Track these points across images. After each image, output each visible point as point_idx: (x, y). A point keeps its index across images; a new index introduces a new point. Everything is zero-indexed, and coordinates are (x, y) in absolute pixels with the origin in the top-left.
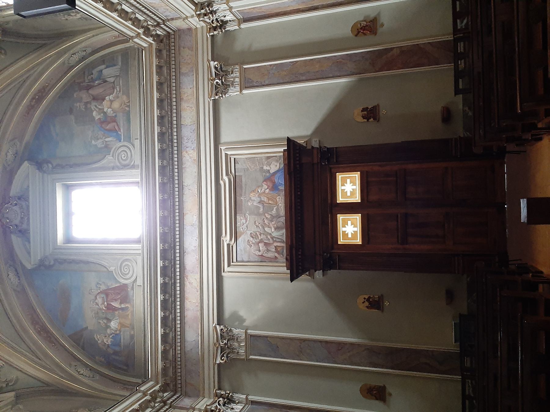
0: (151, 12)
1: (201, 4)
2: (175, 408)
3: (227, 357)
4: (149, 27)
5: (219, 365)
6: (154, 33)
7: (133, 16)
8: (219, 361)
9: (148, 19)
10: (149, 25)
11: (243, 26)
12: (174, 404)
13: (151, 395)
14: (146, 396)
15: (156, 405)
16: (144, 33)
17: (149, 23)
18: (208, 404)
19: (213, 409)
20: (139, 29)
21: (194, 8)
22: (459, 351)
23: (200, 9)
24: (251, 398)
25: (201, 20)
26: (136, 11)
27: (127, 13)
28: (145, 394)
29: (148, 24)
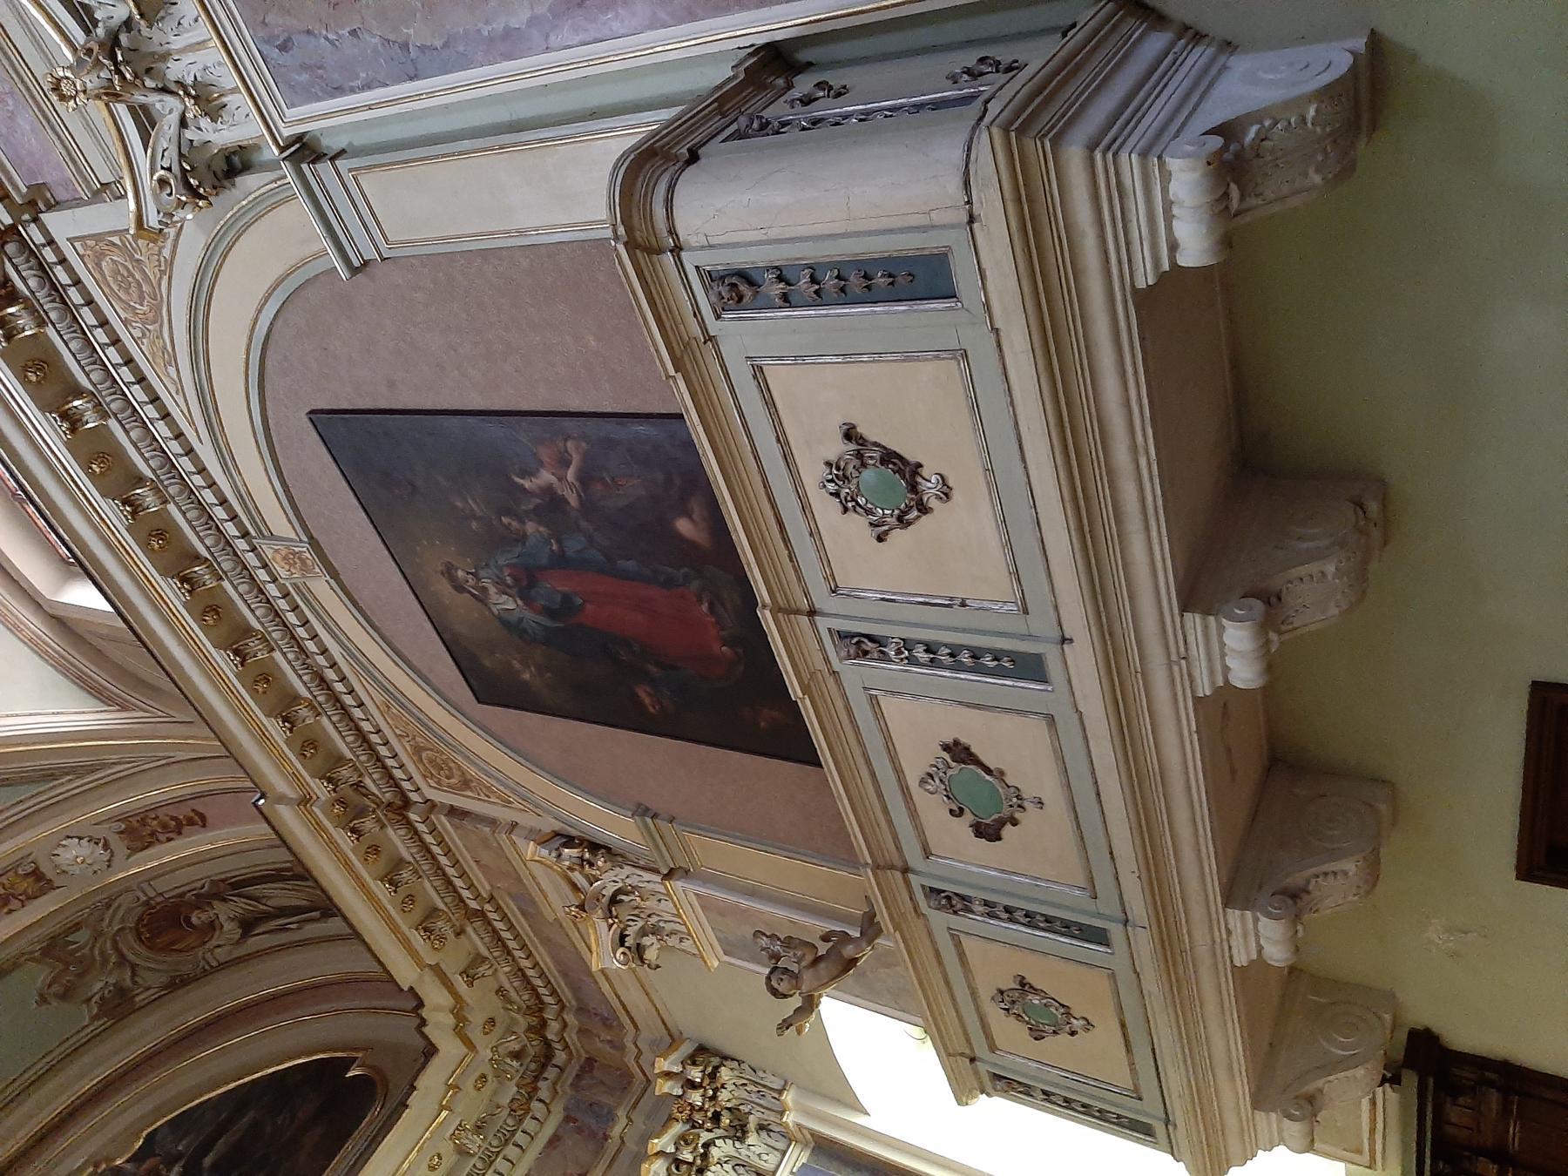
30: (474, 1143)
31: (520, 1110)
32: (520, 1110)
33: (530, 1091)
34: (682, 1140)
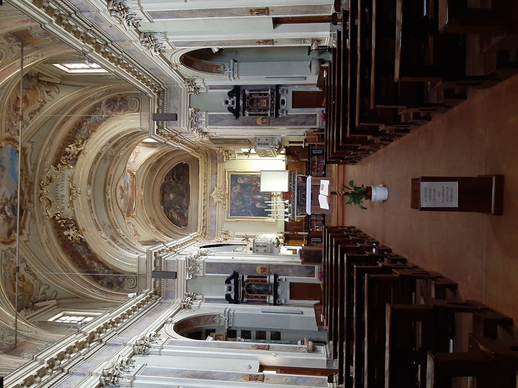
0: (67, 5)
1: (144, 33)
2: (73, 374)
3: (193, 276)
4: (62, 16)
5: (187, 281)
6: (66, 22)
7: (75, 29)
8: (187, 278)
9: (112, 51)
10: (62, 14)
11: (209, 91)
12: (71, 370)
13: (48, 362)
14: (43, 364)
15: (54, 372)
16: (57, 22)
17: (61, 12)
18: (137, 340)
19: (110, 372)
20: (39, 8)
21: (184, 81)
22: (319, 266)
23: (112, 5)
24: (206, 297)
25: (113, 16)
26: (78, 25)
27: (53, 10)
28: (42, 362)
29: (60, 14)
30: (206, 165)
31: (207, 160)
32: (207, 160)
33: (207, 159)
34: (226, 158)
